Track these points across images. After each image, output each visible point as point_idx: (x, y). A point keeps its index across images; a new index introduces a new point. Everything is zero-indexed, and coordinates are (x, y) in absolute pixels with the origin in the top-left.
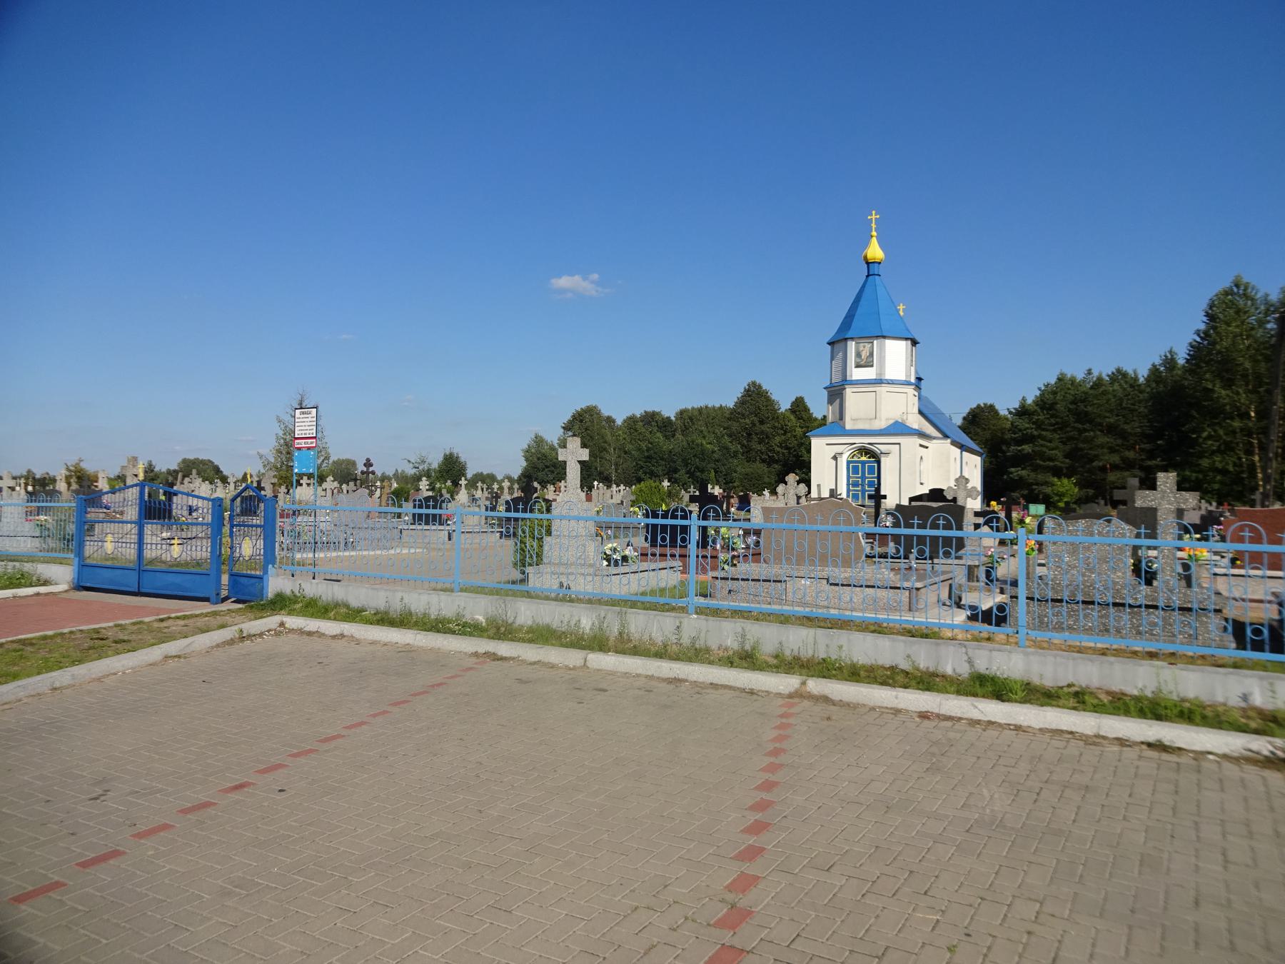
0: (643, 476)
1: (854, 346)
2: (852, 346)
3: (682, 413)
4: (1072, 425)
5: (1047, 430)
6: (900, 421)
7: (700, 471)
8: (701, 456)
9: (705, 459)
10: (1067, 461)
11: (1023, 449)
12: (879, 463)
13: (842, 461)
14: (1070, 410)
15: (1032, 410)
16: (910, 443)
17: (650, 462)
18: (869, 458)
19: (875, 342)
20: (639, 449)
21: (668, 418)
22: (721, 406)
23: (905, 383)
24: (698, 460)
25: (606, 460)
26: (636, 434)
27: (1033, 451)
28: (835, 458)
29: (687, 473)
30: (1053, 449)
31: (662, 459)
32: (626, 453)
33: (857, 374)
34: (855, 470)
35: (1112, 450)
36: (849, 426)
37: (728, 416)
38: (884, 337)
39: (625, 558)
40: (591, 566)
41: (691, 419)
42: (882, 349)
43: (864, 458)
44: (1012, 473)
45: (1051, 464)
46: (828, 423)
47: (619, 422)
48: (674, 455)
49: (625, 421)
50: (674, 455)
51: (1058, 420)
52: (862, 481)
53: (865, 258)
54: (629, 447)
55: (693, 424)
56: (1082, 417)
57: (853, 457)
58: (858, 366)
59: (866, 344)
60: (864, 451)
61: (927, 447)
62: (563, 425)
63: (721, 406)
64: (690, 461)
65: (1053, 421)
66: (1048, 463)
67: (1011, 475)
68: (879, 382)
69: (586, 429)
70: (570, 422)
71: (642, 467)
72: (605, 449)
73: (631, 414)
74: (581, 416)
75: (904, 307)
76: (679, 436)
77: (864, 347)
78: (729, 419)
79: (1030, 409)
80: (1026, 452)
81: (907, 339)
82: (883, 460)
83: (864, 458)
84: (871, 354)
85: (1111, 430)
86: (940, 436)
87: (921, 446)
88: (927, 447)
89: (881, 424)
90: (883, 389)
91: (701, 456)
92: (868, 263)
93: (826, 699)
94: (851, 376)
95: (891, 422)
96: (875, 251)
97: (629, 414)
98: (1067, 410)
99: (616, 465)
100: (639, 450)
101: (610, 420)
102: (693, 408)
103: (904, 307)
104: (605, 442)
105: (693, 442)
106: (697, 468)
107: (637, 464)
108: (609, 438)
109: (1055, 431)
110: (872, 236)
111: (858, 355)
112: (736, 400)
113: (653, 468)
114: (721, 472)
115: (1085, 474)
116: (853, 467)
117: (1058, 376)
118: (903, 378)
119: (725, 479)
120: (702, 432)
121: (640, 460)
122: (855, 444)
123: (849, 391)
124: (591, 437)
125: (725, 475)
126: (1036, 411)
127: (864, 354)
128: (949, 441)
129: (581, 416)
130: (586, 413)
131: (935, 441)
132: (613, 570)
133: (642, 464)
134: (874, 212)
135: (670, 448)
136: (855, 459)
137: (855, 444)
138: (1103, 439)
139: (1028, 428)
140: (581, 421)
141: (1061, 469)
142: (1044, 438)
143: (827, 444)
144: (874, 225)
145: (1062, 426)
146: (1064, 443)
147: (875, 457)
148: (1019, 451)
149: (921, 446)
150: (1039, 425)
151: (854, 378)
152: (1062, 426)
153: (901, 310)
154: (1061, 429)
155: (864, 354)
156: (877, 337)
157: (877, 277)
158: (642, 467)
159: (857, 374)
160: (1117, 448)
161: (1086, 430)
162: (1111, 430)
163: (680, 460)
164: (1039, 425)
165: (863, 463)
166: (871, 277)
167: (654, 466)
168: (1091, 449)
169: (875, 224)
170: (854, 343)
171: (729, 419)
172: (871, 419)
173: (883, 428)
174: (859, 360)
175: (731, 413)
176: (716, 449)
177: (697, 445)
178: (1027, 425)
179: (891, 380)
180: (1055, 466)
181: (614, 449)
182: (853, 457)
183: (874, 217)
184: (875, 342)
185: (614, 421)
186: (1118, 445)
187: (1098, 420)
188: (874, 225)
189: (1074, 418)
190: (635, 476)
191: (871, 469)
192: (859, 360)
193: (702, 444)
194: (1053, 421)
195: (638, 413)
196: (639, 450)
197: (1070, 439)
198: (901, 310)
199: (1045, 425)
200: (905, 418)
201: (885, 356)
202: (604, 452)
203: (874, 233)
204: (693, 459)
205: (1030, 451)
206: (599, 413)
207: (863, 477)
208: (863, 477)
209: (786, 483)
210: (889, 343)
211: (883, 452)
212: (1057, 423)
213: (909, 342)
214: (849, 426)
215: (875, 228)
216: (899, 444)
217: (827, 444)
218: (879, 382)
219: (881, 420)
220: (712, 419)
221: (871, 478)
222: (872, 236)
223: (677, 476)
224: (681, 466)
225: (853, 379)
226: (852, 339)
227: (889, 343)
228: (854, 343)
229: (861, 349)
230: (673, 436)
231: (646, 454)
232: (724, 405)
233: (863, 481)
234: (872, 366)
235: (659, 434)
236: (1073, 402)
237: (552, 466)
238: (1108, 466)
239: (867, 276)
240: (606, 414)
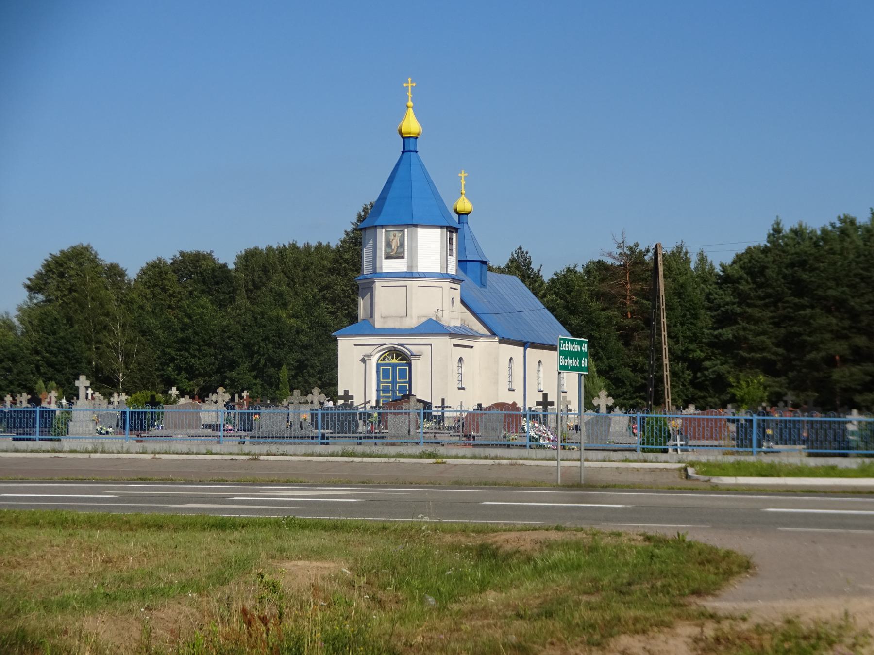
0: (174, 375)
1: (383, 234)
2: (382, 234)
3: (249, 258)
4: (735, 306)
5: (756, 306)
6: (434, 319)
7: (273, 366)
8: (276, 339)
9: (284, 345)
10: (781, 350)
11: (720, 335)
12: (410, 365)
13: (370, 364)
14: (785, 277)
15: (736, 276)
16: (442, 344)
17: (187, 350)
18: (401, 360)
19: (406, 230)
20: (167, 327)
21: (225, 266)
22: (320, 244)
23: (441, 275)
24: (271, 345)
25: (108, 346)
26: (164, 296)
27: (734, 336)
28: (363, 361)
29: (251, 370)
30: (759, 334)
31: (209, 345)
32: (143, 333)
33: (388, 266)
34: (386, 374)
35: (839, 336)
36: (379, 324)
37: (329, 266)
38: (416, 226)
39: (107, 433)
40: (91, 434)
41: (265, 270)
42: (413, 238)
43: (395, 361)
44: (707, 369)
45: (758, 355)
46: (359, 320)
47: (132, 272)
48: (229, 338)
49: (144, 272)
50: (229, 338)
51: (770, 290)
52: (393, 386)
53: (400, 132)
54: (151, 322)
55: (269, 279)
56: (799, 288)
57: (384, 360)
58: (387, 257)
59: (396, 233)
60: (395, 352)
61: (472, 347)
62: (28, 283)
63: (320, 244)
64: (256, 348)
65: (760, 292)
66: (752, 354)
67: (706, 373)
68: (409, 275)
69: (71, 290)
70: (40, 276)
71: (172, 359)
72: (106, 327)
73: (155, 258)
74: (61, 266)
75: (466, 175)
76: (242, 300)
77: (395, 236)
78: (331, 271)
79: (733, 276)
80: (725, 338)
81: (442, 227)
82: (414, 362)
83: (395, 361)
84: (402, 245)
85: (838, 306)
86: (488, 333)
87: (455, 345)
88: (472, 347)
89: (411, 322)
90: (414, 284)
91: (276, 339)
92: (404, 138)
93: (160, 458)
94: (381, 268)
95: (424, 320)
96: (411, 124)
97: (152, 258)
98: (781, 276)
99: (127, 355)
100: (169, 328)
101: (115, 271)
102: (270, 249)
103: (466, 175)
104: (107, 315)
105: (262, 314)
106: (269, 359)
107: (164, 353)
108: (113, 307)
109: (766, 306)
110: (408, 107)
111: (388, 244)
112: (343, 236)
113: (193, 360)
114: (312, 367)
115: (804, 370)
116: (383, 371)
117: (773, 225)
118: (438, 270)
119: (320, 379)
120: (280, 295)
121: (169, 347)
122: (385, 344)
123: (378, 285)
124: (80, 305)
125: (321, 372)
126: (741, 278)
127: (395, 244)
128: (497, 339)
129: (61, 266)
130: (70, 260)
131: (482, 339)
132: (101, 436)
133: (173, 353)
134: (410, 79)
135: (225, 323)
136: (387, 361)
137: (385, 344)
138: (823, 320)
139: (728, 304)
140: (61, 275)
141: (774, 363)
142: (749, 319)
143: (355, 345)
144: (410, 95)
145: (777, 300)
146: (777, 325)
147: (404, 357)
148: (716, 336)
149: (455, 345)
150: (743, 299)
151: (385, 270)
152: (777, 300)
153: (463, 178)
154: (775, 304)
155: (395, 244)
156: (407, 226)
157: (412, 154)
158: (172, 359)
159: (388, 266)
160: (845, 332)
161: (803, 307)
162: (838, 306)
163: (239, 346)
164: (743, 299)
165: (394, 366)
166: (406, 154)
167: (194, 356)
168: (810, 334)
169: (412, 93)
170: (384, 231)
171: (331, 271)
172: (401, 317)
173: (413, 327)
174: (388, 250)
175: (335, 261)
176: (305, 326)
177: (271, 320)
178: (728, 299)
179: (423, 273)
180: (764, 358)
181: (123, 326)
182: (384, 360)
183: (410, 85)
184: (406, 230)
185: (122, 274)
186: (844, 328)
187: (820, 292)
188: (410, 95)
189: (790, 289)
190: (162, 375)
191: (402, 372)
192: (388, 250)
193: (278, 319)
194: (760, 292)
195: (168, 255)
196: (169, 328)
197: (787, 318)
198: (463, 178)
199: (751, 299)
200: (440, 314)
201: (416, 247)
202: (105, 333)
203: (410, 104)
204: (262, 344)
205: (730, 336)
206: (93, 260)
207: (394, 382)
208: (394, 382)
209: (217, 393)
210: (420, 231)
211: (415, 354)
212: (768, 296)
213: (445, 230)
214: (379, 324)
215: (411, 98)
216: (430, 345)
217: (355, 345)
218: (409, 275)
219: (412, 318)
220: (303, 270)
221: (401, 382)
222: (408, 107)
223: (234, 374)
224: (241, 357)
225: (383, 271)
226: (382, 227)
227: (422, 233)
228: (384, 231)
229: (392, 237)
230: (232, 300)
231: (180, 335)
232: (324, 243)
233: (394, 386)
234: (403, 257)
235: (205, 300)
236: (792, 265)
237: (9, 359)
238: (837, 358)
239: (403, 152)
240: (108, 262)
